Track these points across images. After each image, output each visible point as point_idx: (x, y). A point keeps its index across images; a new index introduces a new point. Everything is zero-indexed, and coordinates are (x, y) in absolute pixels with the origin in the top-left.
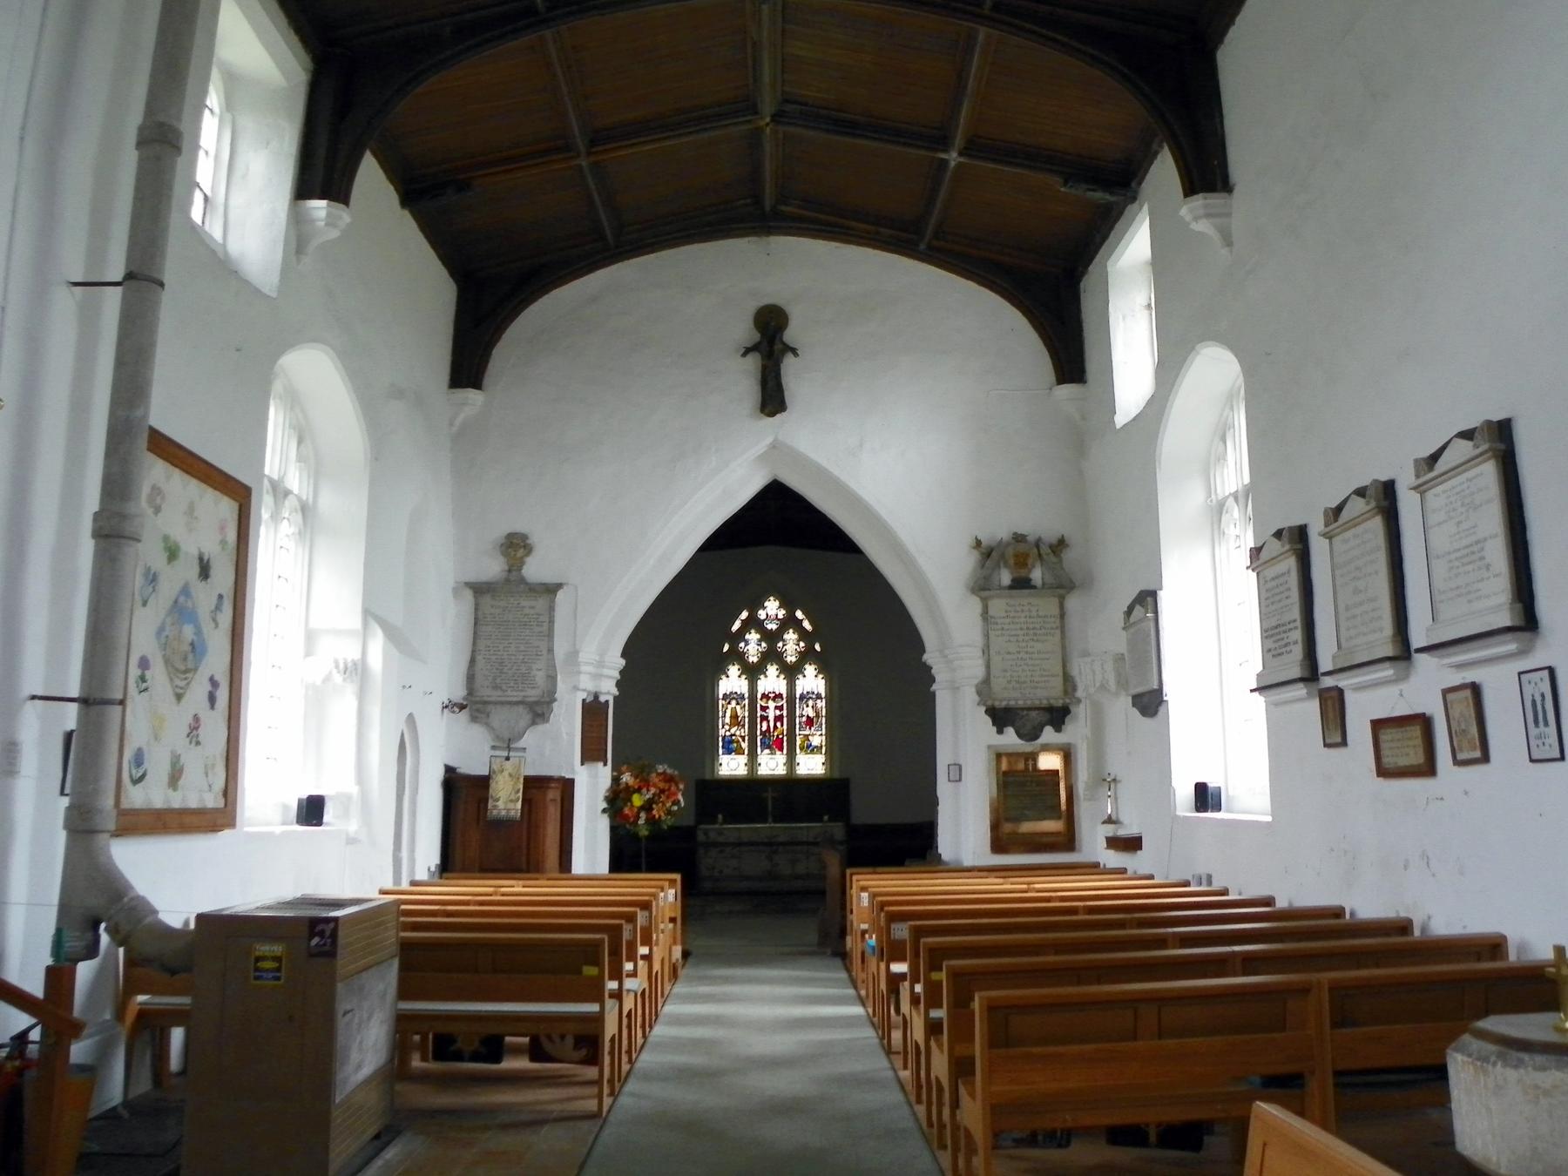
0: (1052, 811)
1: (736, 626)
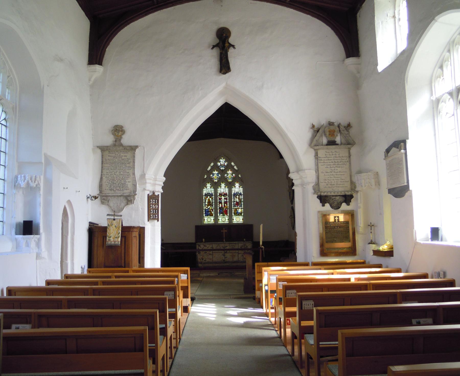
0: (345, 238)
1: (209, 168)
